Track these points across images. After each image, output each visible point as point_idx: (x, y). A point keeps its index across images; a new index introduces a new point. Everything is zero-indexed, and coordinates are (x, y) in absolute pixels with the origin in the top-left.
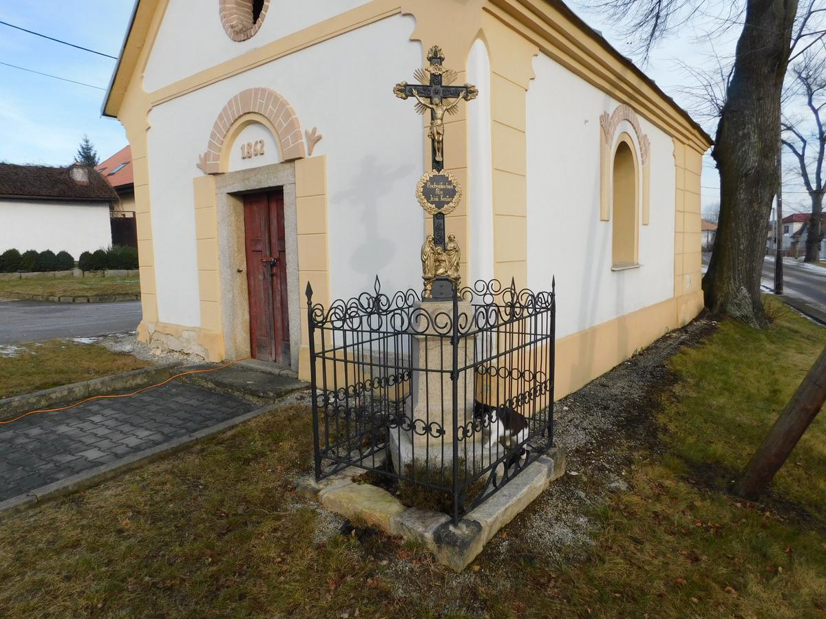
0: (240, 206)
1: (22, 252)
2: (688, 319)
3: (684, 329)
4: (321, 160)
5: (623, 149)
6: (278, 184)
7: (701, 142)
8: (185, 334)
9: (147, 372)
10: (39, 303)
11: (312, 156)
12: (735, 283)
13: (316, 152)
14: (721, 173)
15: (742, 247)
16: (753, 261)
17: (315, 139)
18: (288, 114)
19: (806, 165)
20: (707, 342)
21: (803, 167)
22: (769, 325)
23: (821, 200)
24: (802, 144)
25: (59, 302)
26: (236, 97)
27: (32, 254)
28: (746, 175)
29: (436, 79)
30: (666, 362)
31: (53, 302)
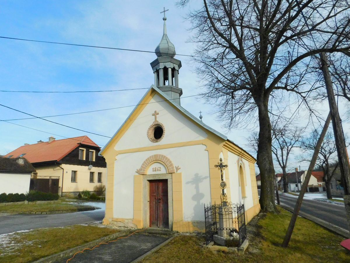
0: (149, 183)
1: (7, 194)
2: (258, 213)
3: (258, 215)
4: (180, 174)
5: (241, 166)
6: (166, 179)
7: (254, 161)
8: (127, 221)
9: (125, 232)
10: (28, 215)
11: (177, 172)
12: (268, 201)
13: (179, 171)
14: (260, 169)
15: (269, 190)
16: (272, 194)
17: (178, 169)
18: (170, 162)
19: (279, 157)
20: (265, 218)
21: (278, 158)
22: (279, 214)
23: (285, 170)
24: (276, 151)
25: (35, 214)
26: (152, 156)
27: (11, 195)
28: (267, 170)
29: (221, 164)
30: (258, 224)
31: (33, 214)
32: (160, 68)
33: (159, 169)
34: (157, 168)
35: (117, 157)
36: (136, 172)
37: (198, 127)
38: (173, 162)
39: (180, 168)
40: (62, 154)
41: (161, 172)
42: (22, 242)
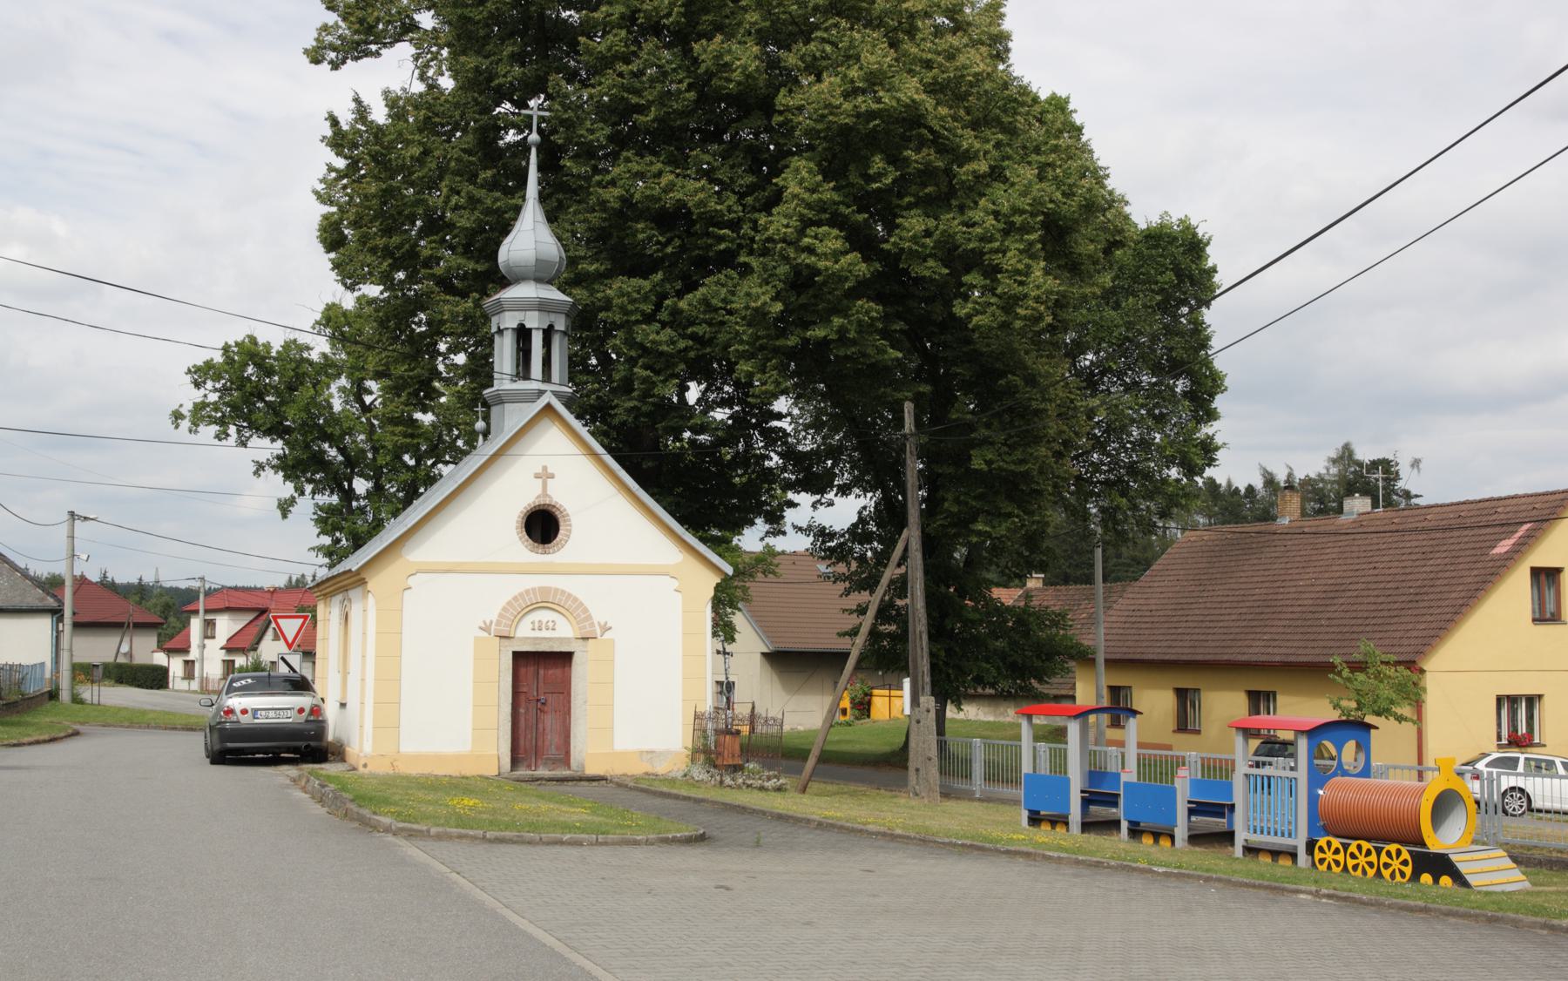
4: (613, 641)
13: (608, 635)
17: (606, 629)
26: (534, 589)
32: (507, 326)
33: (551, 625)
35: (411, 581)
36: (481, 628)
38: (592, 611)
39: (610, 628)
40: (1136, 589)
41: (550, 632)
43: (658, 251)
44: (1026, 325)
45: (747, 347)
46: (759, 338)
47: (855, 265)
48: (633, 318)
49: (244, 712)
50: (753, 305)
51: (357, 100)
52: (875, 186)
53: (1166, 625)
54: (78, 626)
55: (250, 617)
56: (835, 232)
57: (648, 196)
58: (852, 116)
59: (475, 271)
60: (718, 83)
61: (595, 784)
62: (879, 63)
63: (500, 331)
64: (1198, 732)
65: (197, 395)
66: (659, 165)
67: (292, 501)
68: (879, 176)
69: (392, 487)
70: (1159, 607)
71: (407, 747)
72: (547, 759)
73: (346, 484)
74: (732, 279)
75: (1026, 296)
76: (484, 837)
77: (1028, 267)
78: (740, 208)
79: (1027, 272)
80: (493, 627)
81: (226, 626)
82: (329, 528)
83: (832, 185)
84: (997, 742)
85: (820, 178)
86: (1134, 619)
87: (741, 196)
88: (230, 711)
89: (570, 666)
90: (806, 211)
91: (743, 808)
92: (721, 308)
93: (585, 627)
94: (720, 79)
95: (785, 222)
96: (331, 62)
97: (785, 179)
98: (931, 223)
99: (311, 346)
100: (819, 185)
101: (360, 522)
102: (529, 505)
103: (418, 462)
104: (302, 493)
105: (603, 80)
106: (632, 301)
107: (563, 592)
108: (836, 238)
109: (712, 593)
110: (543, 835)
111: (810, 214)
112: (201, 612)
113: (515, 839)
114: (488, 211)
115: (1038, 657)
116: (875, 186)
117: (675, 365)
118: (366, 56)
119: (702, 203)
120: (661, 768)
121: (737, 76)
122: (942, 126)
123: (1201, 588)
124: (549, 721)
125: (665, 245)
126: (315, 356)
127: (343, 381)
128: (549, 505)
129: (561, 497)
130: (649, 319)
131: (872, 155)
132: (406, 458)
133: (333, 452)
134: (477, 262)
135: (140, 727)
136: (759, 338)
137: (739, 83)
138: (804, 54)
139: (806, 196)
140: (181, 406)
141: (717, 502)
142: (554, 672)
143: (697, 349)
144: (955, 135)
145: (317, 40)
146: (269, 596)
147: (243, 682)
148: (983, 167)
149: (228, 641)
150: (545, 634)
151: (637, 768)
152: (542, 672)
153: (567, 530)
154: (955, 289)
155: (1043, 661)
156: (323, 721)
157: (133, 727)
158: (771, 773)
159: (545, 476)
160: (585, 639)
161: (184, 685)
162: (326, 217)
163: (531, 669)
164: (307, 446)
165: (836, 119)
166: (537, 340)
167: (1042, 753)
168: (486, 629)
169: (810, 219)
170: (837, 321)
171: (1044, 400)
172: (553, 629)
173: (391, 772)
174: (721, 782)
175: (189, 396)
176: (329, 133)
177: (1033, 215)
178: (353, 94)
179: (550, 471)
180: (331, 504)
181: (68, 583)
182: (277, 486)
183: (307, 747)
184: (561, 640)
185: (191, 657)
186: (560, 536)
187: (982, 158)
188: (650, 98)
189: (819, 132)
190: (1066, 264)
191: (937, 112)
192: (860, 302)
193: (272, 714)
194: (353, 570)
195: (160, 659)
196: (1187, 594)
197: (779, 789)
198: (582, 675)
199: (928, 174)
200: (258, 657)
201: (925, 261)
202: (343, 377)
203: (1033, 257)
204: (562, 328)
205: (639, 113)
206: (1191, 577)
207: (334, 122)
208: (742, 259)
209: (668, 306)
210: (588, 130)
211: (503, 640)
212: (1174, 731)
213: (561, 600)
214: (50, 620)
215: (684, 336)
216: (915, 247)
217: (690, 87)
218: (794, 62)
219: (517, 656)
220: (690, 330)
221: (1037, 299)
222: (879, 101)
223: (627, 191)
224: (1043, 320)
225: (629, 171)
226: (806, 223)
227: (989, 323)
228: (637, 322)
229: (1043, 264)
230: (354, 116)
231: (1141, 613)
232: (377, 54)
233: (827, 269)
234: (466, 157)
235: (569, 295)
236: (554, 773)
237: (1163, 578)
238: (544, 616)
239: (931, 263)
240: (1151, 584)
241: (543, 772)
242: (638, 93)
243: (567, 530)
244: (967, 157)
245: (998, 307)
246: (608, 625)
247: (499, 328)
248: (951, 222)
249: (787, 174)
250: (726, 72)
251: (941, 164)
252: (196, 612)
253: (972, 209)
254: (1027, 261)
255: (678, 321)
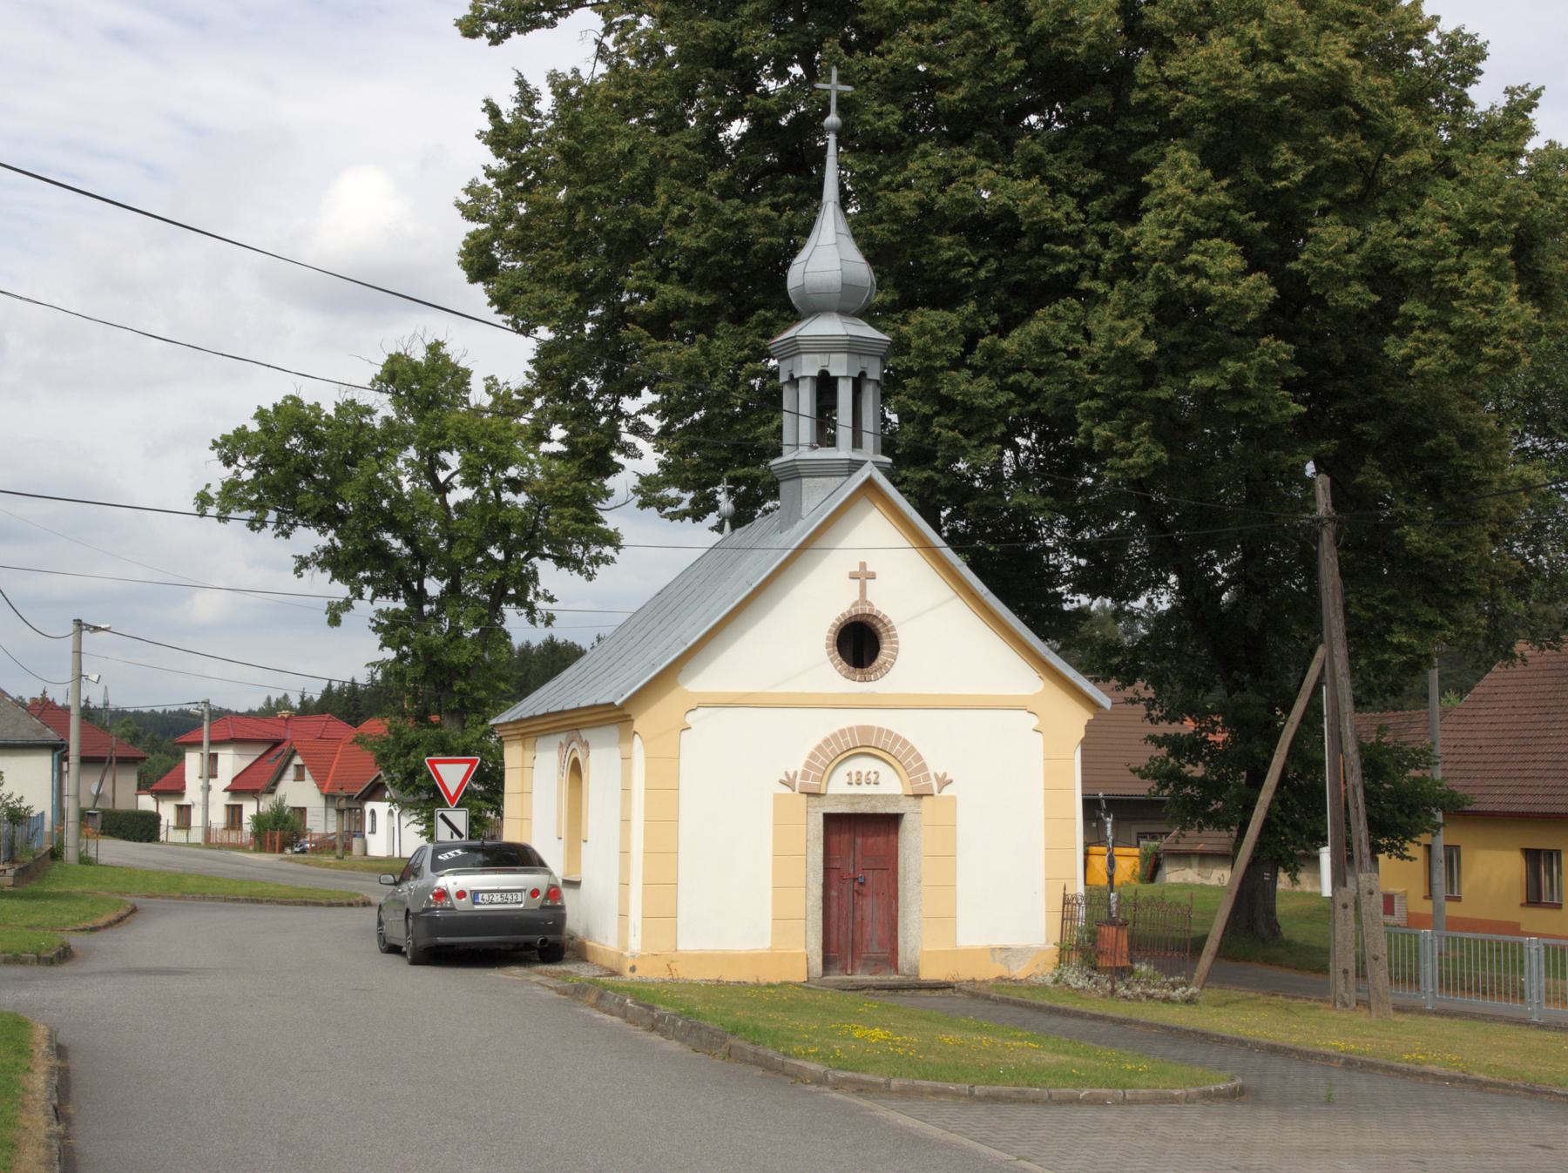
4: (954, 798)
11: (942, 794)
13: (947, 791)
17: (944, 782)
26: (851, 729)
32: (804, 374)
33: (873, 777)
34: (864, 774)
36: (782, 782)
37: (685, 668)
39: (951, 782)
42: (949, 15)
43: (969, 275)
44: (1495, 369)
45: (1101, 403)
46: (1122, 388)
47: (1258, 290)
48: (938, 364)
49: (461, 894)
50: (1121, 343)
51: (521, 83)
52: (1279, 184)
53: (1506, 766)
54: (86, 761)
55: (260, 751)
56: (1229, 246)
57: (958, 200)
58: (1253, 89)
59: (698, 305)
60: (1061, 47)
61: (937, 993)
62: (1291, 17)
63: (794, 381)
64: (1559, 906)
65: (228, 473)
66: (972, 159)
67: (347, 605)
68: (1284, 172)
69: (474, 587)
70: (1492, 742)
71: (687, 944)
72: (866, 959)
73: (415, 584)
74: (1074, 310)
75: (1494, 330)
76: (972, 1093)
77: (1497, 291)
78: (1082, 216)
79: (1496, 298)
80: (798, 781)
81: (231, 763)
82: (397, 640)
83: (1225, 183)
84: (1460, 934)
85: (1208, 173)
86: (1457, 758)
87: (1083, 200)
88: (442, 894)
89: (896, 833)
90: (1193, 219)
91: (1202, 1034)
92: (1061, 350)
93: (917, 780)
94: (1063, 41)
95: (1164, 232)
96: (491, 35)
97: (1160, 176)
98: (1355, 234)
99: (374, 408)
100: (1207, 184)
101: (433, 632)
102: (843, 615)
103: (508, 556)
104: (360, 596)
105: (894, 46)
106: (936, 341)
107: (889, 733)
108: (1232, 252)
109: (1082, 734)
110: (1053, 1091)
111: (1198, 223)
112: (206, 744)
113: (1014, 1096)
114: (728, 225)
115: (1401, 811)
116: (1279, 184)
117: (993, 426)
118: (538, 26)
119: (1034, 210)
120: (1019, 971)
121: (1089, 36)
122: (1371, 102)
123: (1550, 718)
124: (870, 908)
125: (977, 267)
126: (377, 422)
127: (412, 453)
128: (869, 615)
129: (885, 603)
130: (957, 363)
131: (1276, 142)
132: (493, 551)
133: (397, 544)
134: (700, 293)
135: (194, 898)
136: (1122, 388)
137: (1091, 47)
138: (1175, 9)
139: (1192, 198)
140: (208, 486)
141: (512, 591)
142: (876, 842)
143: (1019, 405)
144: (1390, 115)
145: (473, 7)
146: (283, 723)
147: (451, 854)
148: (1423, 157)
149: (234, 780)
150: (865, 789)
151: (987, 972)
152: (859, 841)
153: (892, 649)
154: (1383, 320)
155: (1408, 816)
156: (562, 907)
157: (185, 898)
158: (1178, 978)
159: (863, 576)
160: (918, 796)
161: (179, 836)
162: (473, 236)
163: (845, 837)
164: (366, 535)
165: (1234, 94)
166: (845, 393)
167: (1533, 951)
168: (788, 783)
169: (1197, 229)
170: (1232, 366)
171: (1488, 468)
172: (876, 783)
173: (667, 978)
174: (1113, 991)
175: (217, 475)
176: (488, 127)
177: (1506, 220)
178: (516, 75)
179: (869, 569)
180: (396, 610)
181: (74, 712)
182: (325, 587)
183: (544, 942)
184: (887, 798)
185: (186, 801)
186: (881, 658)
187: (1422, 145)
188: (963, 68)
189: (1204, 111)
190: (1531, 287)
191: (1366, 84)
192: (1266, 340)
193: (497, 898)
194: (617, 703)
195: (146, 803)
196: (1531, 726)
197: (1189, 1001)
198: (914, 845)
199: (1340, 172)
200: (282, 801)
201: (1347, 285)
202: (411, 448)
203: (1503, 278)
204: (877, 376)
205: (943, 88)
206: (1532, 704)
207: (493, 111)
208: (1085, 284)
209: (984, 346)
210: (874, 114)
211: (811, 798)
212: (1522, 905)
213: (846, 743)
214: (50, 758)
215: (1004, 387)
216: (1337, 267)
217: (1018, 54)
218: (1164, 18)
219: (830, 820)
220: (1011, 379)
221: (1512, 335)
222: (1291, 68)
223: (928, 194)
224: (1519, 363)
225: (929, 167)
226: (1193, 235)
227: (1438, 368)
228: (942, 368)
229: (1515, 287)
230: (517, 105)
231: (1466, 750)
232: (551, 24)
233: (1223, 295)
234: (691, 154)
235: (883, 330)
236: (874, 978)
237: (1492, 705)
238: (865, 765)
239: (1356, 287)
240: (1474, 712)
241: (861, 977)
242: (942, 62)
243: (892, 649)
244: (1405, 144)
245: (1451, 347)
246: (947, 778)
247: (791, 376)
248: (1381, 231)
249: (1162, 168)
250: (1070, 32)
251: (1368, 153)
252: (199, 744)
253: (1407, 214)
254: (1494, 283)
255: (997, 367)
